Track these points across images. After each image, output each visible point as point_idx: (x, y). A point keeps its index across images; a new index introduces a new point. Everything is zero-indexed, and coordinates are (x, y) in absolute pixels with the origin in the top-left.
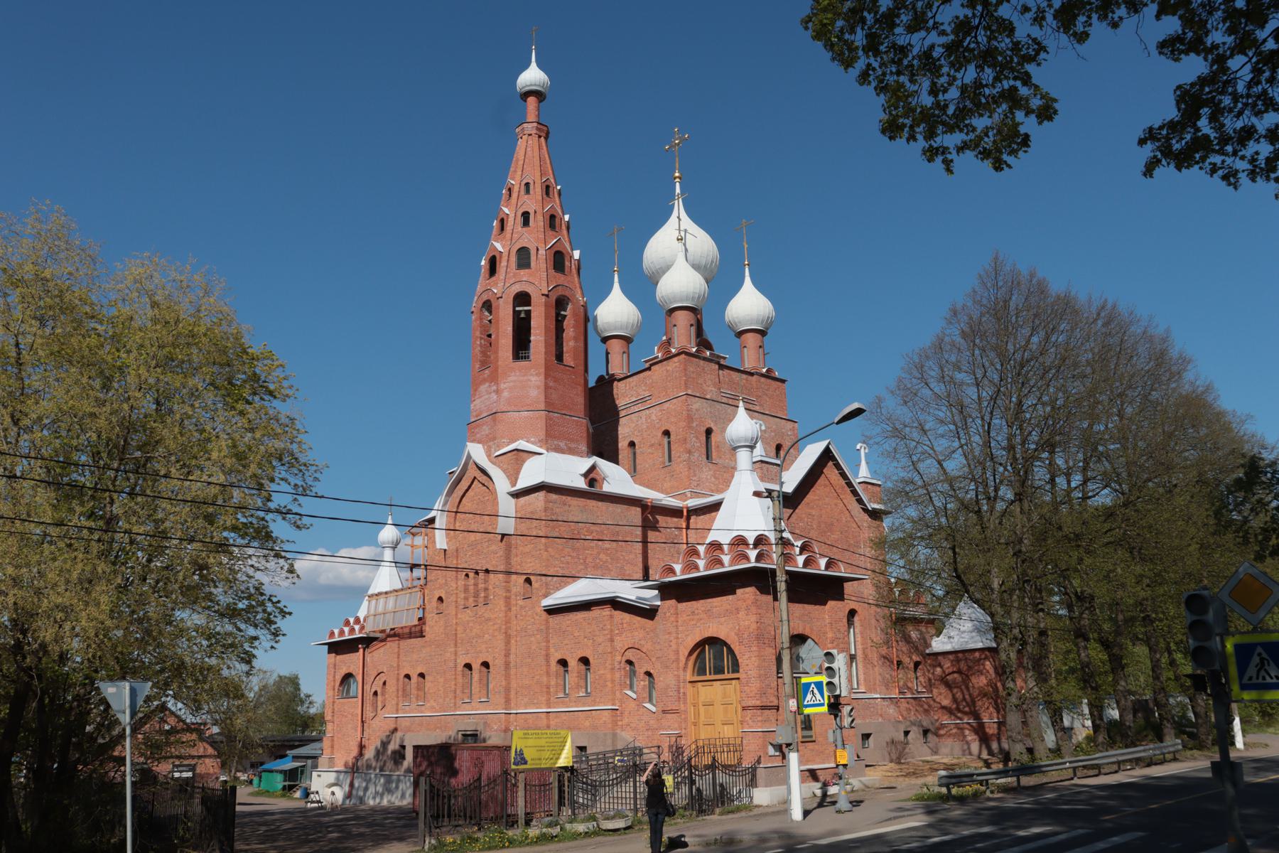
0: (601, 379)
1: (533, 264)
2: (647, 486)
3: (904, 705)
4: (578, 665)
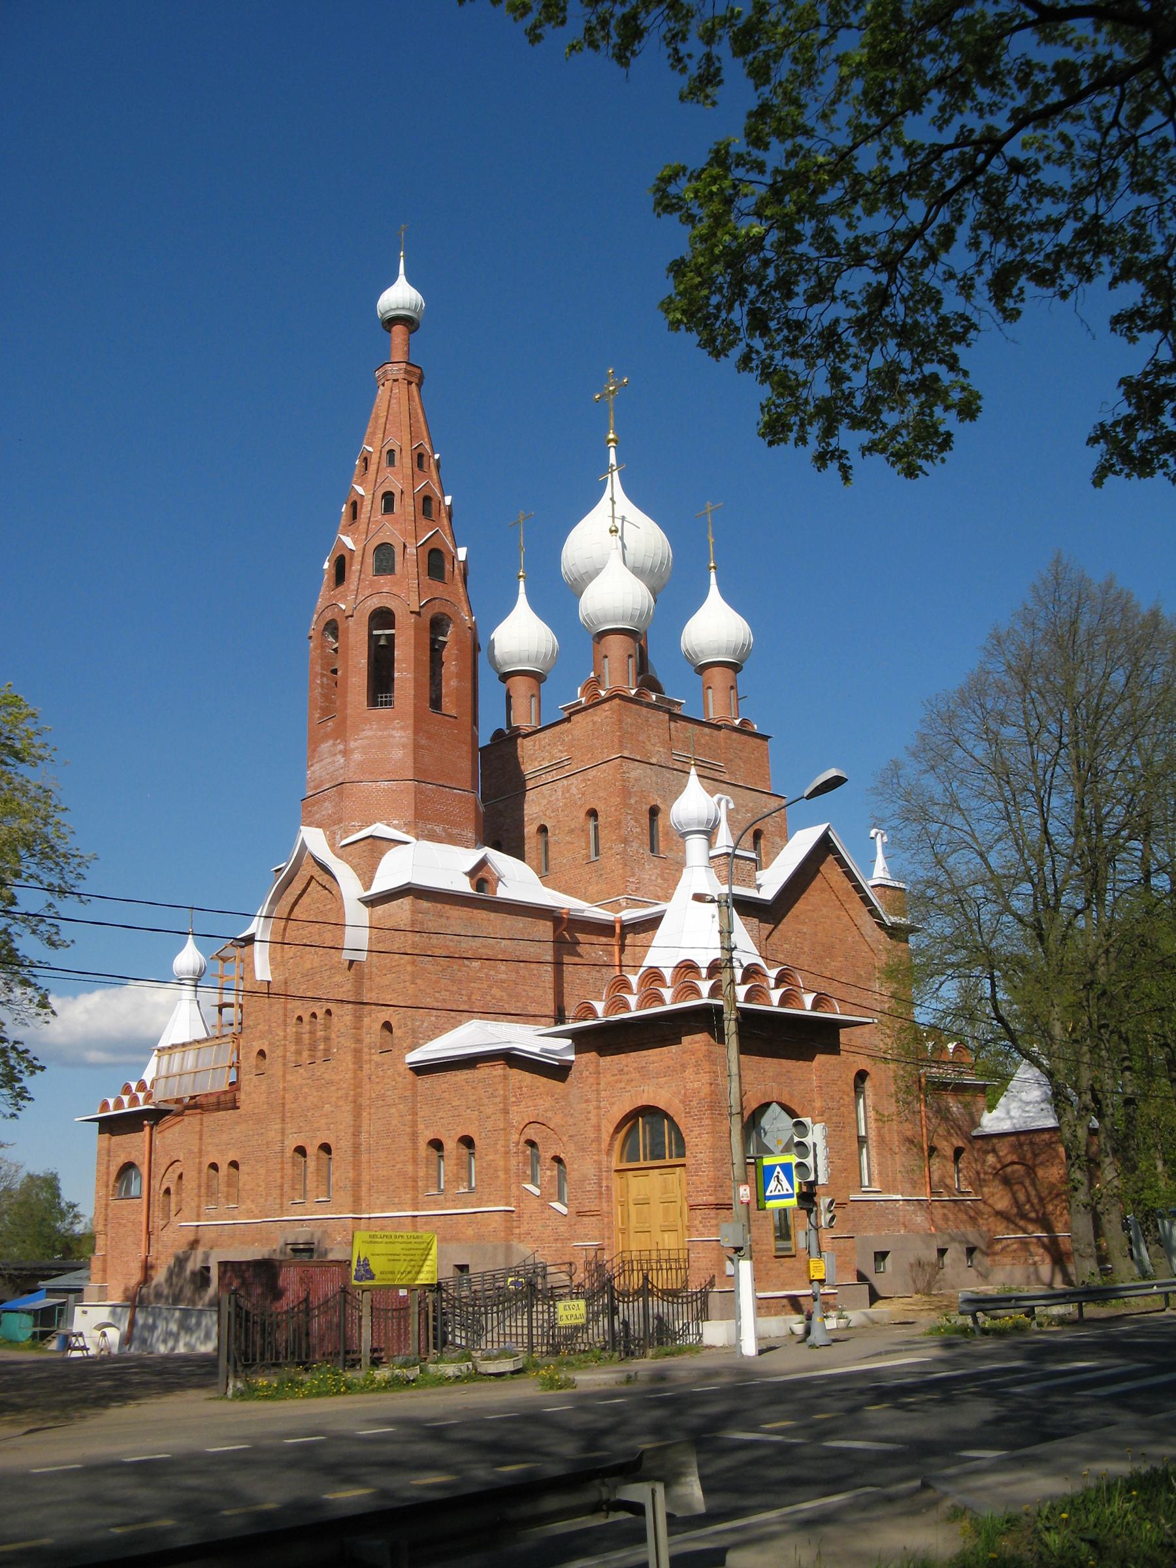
0: (498, 734)
1: (398, 568)
2: (564, 892)
3: (938, 1212)
4: (458, 1148)
